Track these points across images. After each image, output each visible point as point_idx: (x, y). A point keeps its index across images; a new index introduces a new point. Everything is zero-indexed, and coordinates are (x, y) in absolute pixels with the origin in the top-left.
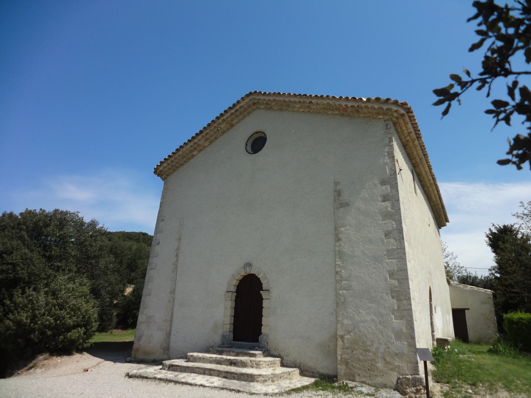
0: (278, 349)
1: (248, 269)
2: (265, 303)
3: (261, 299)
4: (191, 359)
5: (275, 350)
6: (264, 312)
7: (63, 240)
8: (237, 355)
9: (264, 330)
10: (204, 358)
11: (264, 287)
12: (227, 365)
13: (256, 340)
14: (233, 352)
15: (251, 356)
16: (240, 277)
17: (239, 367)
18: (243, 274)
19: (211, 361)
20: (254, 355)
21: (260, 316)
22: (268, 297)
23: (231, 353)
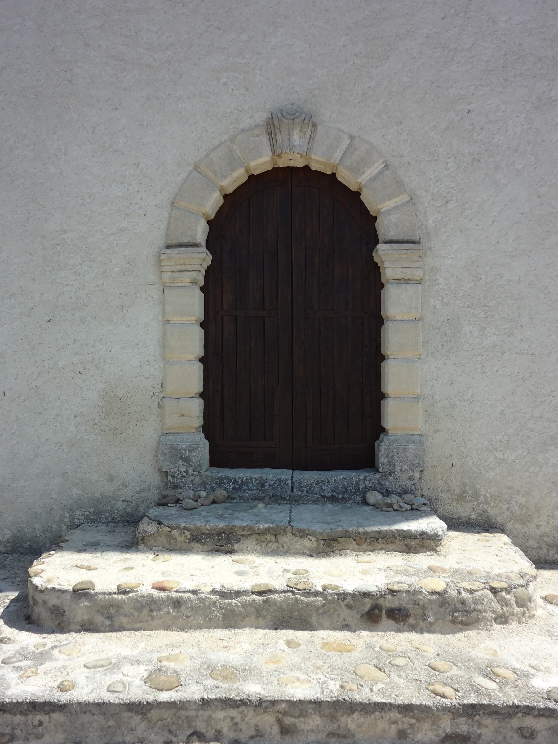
0: (476, 495)
1: (297, 138)
2: (397, 303)
3: (372, 281)
4: (81, 611)
5: (461, 498)
6: (393, 340)
7: (438, 709)
8: (329, 545)
9: (394, 416)
10: (177, 603)
11: (386, 227)
12: (345, 627)
13: (367, 460)
14: (302, 534)
15: (409, 550)
16: (233, 180)
17: (430, 630)
18: (262, 162)
19: (228, 611)
20: (426, 543)
21: (372, 358)
22: (417, 274)
23: (286, 539)
